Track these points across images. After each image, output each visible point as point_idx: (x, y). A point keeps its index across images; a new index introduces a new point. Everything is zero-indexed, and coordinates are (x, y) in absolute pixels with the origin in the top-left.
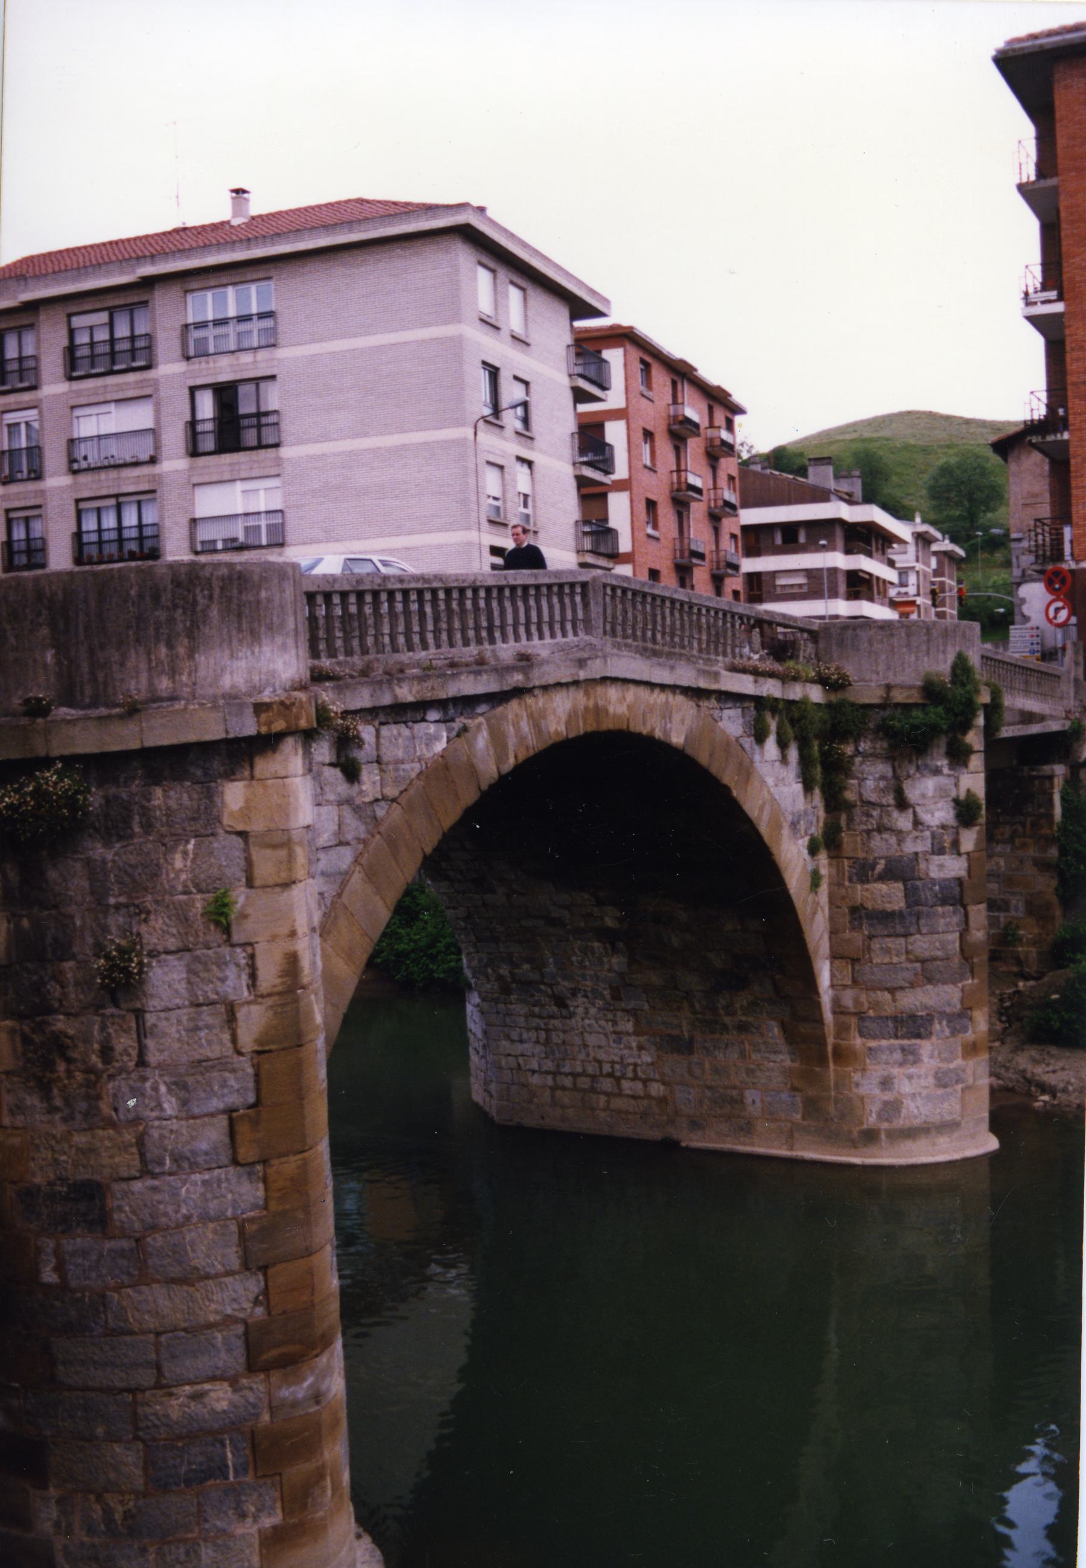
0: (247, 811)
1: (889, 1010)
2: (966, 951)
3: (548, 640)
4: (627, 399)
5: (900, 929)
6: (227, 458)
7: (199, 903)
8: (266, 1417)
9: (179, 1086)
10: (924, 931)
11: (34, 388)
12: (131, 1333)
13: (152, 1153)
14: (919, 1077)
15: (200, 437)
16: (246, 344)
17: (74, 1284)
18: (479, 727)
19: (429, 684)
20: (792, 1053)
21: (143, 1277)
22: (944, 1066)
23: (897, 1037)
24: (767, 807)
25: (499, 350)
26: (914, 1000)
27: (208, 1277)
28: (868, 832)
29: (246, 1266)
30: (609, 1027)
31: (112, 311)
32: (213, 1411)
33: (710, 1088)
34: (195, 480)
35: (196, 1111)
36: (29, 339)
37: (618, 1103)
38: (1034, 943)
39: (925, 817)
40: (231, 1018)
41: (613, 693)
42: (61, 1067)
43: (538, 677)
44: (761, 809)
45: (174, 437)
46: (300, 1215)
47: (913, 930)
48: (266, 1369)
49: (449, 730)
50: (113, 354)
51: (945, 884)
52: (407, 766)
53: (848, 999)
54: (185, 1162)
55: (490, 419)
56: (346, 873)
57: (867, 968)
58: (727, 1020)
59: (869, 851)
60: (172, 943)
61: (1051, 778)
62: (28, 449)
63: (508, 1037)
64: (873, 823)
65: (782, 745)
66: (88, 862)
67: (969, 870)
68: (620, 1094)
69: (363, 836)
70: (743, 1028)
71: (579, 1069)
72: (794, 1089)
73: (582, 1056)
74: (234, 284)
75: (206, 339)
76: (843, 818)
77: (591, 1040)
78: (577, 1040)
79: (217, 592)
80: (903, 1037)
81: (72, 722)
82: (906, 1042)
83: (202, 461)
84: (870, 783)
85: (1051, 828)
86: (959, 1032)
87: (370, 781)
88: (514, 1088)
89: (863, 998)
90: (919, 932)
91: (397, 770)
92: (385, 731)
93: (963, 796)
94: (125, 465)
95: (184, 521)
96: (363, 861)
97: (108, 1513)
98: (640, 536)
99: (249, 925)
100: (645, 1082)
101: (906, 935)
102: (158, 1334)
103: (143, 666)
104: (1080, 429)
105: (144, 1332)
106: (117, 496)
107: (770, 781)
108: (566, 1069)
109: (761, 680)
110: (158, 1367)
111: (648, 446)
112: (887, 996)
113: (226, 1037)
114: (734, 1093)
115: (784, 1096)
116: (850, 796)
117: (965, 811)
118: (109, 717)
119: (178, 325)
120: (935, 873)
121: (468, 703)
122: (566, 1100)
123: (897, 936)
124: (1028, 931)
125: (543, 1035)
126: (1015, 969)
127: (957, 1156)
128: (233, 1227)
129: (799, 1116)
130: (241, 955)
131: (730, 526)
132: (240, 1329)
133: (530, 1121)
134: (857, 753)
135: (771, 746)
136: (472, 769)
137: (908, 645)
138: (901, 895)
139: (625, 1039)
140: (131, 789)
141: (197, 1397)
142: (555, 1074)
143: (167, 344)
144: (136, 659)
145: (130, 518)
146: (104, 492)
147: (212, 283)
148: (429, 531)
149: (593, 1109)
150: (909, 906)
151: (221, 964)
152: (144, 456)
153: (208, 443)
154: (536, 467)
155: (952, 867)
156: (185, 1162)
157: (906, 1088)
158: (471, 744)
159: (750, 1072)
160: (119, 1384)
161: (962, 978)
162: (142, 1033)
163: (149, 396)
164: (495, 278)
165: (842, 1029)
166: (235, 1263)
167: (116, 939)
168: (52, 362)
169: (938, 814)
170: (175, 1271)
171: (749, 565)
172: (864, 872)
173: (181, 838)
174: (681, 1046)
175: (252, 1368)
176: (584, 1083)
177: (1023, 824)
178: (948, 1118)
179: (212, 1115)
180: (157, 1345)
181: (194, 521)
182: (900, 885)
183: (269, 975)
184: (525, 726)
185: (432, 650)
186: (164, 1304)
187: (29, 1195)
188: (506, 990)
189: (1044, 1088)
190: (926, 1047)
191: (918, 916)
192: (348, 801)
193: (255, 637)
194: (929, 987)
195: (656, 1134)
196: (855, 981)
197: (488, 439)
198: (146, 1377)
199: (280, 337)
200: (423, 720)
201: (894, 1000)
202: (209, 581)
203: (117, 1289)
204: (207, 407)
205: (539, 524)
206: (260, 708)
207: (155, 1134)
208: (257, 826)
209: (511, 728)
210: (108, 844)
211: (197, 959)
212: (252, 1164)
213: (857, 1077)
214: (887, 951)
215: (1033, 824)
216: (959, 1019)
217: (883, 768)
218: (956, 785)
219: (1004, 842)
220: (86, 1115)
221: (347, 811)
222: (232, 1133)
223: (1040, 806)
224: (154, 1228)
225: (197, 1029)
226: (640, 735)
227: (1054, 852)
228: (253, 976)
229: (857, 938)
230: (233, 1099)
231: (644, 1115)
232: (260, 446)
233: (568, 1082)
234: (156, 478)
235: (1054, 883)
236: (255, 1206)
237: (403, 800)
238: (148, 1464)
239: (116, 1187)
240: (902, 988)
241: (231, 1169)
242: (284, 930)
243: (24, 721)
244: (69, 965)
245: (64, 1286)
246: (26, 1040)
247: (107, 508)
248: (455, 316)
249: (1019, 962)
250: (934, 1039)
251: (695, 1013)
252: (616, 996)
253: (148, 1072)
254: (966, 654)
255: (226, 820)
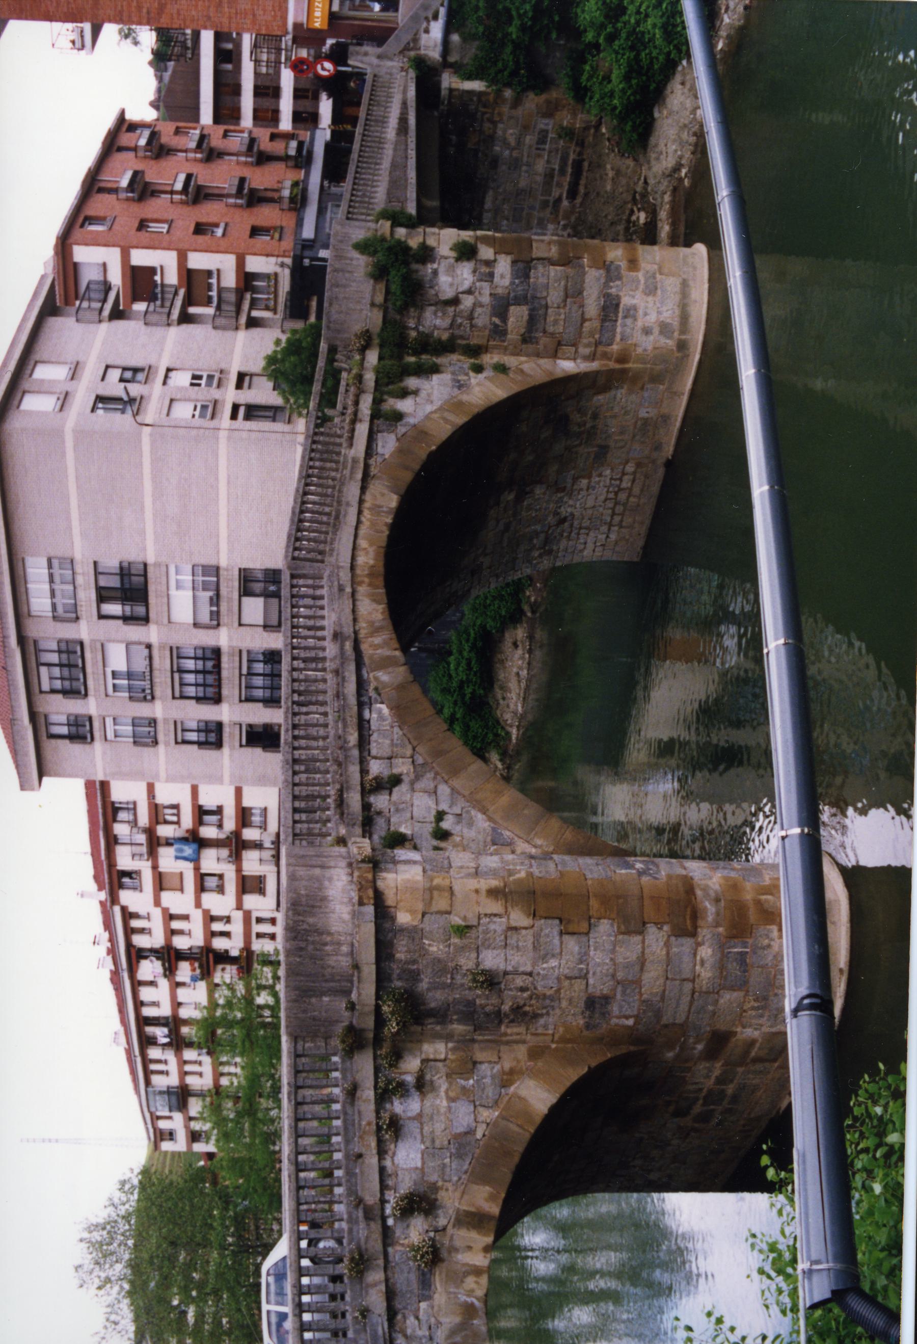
0: (412, 912)
1: (596, 324)
2: (564, 261)
3: (325, 612)
4: (114, 246)
5: (541, 312)
6: (152, 599)
7: (455, 940)
8: (721, 929)
9: (544, 958)
10: (545, 294)
11: (90, 719)
12: (664, 991)
13: (576, 973)
14: (646, 307)
15: (135, 614)
16: (70, 578)
17: (635, 1013)
18: (376, 679)
19: (349, 719)
20: (617, 388)
21: (638, 983)
22: (642, 287)
23: (616, 321)
24: (446, 414)
25: (83, 397)
26: (592, 307)
27: (643, 953)
28: (472, 326)
29: (641, 933)
30: (583, 493)
31: (39, 664)
32: (712, 956)
33: (634, 436)
34: (165, 621)
35: (558, 951)
36: (54, 718)
37: (636, 490)
38: (574, 115)
39: (466, 285)
40: (516, 929)
41: (361, 559)
42: (527, 1008)
43: (348, 630)
44: (446, 421)
45: (135, 632)
46: (621, 901)
47: (544, 303)
48: (695, 927)
49: (376, 702)
50: (70, 666)
51: (516, 274)
52: (396, 736)
53: (584, 351)
54: (583, 958)
55: (135, 408)
56: (453, 789)
57: (565, 336)
58: (588, 425)
59: (485, 327)
60: (474, 955)
61: (451, 90)
62: (134, 725)
63: (581, 551)
64: (466, 323)
65: (404, 394)
66: (429, 989)
67: (507, 253)
68: (631, 489)
69: (432, 775)
70: (595, 416)
71: (610, 511)
72: (642, 388)
73: (601, 509)
74: (26, 582)
75: (64, 604)
76: (459, 342)
77: (590, 503)
78: (590, 512)
79: (301, 918)
80: (617, 316)
81: (359, 994)
82: (620, 315)
83: (152, 615)
84: (438, 322)
85: (488, 94)
86: (619, 273)
87: (403, 767)
88: (617, 549)
89: (585, 341)
90: (545, 298)
91: (397, 745)
92: (374, 752)
93: (453, 254)
94: (151, 665)
95: (195, 631)
96: (446, 778)
97: (753, 1008)
98: (224, 244)
99: (470, 915)
100: (624, 474)
101: (547, 307)
102: (667, 978)
103: (335, 958)
104: (184, 20)
105: (665, 985)
106: (172, 672)
107: (429, 408)
108: (609, 519)
109: (360, 415)
110: (684, 980)
111: (151, 225)
112: (587, 324)
113: (524, 932)
114: (639, 423)
115: (646, 394)
116: (445, 336)
117: (466, 252)
118: (359, 977)
119: (52, 623)
120: (506, 282)
121: (361, 684)
122: (630, 520)
123: (546, 314)
124: (565, 119)
125: (582, 531)
126: (592, 131)
127: (706, 286)
128: (620, 937)
129: (661, 387)
130: (484, 920)
131: (216, 141)
132: (673, 939)
133: (641, 543)
134: (416, 329)
135: (405, 405)
136: (400, 688)
137: (345, 286)
138: (518, 308)
139: (593, 484)
140: (396, 969)
141: (703, 963)
142: (610, 525)
143: (67, 632)
144: (332, 961)
145: (190, 664)
146: (169, 680)
147: (24, 597)
148: (217, 465)
149: (638, 505)
150: (527, 304)
151: (486, 932)
152: (146, 652)
153: (140, 610)
154: (171, 366)
155: (504, 267)
156: (583, 958)
157: (652, 318)
158: (385, 685)
159: (626, 413)
160: (689, 998)
161: (582, 267)
162: (516, 972)
163: (102, 645)
164: (29, 392)
165: (606, 356)
166: (638, 938)
167: (467, 981)
168: (75, 706)
169: (465, 276)
170: (637, 968)
171: (247, 120)
172: (499, 332)
173: (422, 947)
174: (603, 452)
175: (693, 934)
176: (619, 509)
177: (484, 113)
178: (678, 289)
179: (561, 943)
180: (673, 980)
181: (196, 625)
182: (512, 308)
183: (495, 907)
184: (377, 640)
185: (328, 709)
186: (653, 974)
187: (588, 1026)
188: (550, 552)
189: (677, 168)
190: (626, 301)
191: (534, 297)
192: (412, 783)
193: (324, 899)
194: (585, 293)
195: (661, 472)
196: (573, 345)
197: (151, 413)
198: (688, 986)
199: (66, 555)
200: (369, 722)
201: (590, 320)
202: (295, 922)
203: (641, 994)
204: (114, 608)
205: (214, 368)
206: (361, 903)
207: (567, 971)
208: (420, 907)
209: (379, 651)
210: (421, 981)
211: (483, 944)
212: (590, 925)
213: (639, 350)
214: (556, 322)
215: (485, 106)
216: (611, 272)
217: (429, 313)
218: (446, 258)
219: (495, 127)
220: (552, 1000)
221: (419, 785)
222: (573, 934)
223: (472, 100)
224: (613, 976)
225: (517, 947)
226: (389, 537)
227: (508, 93)
228: (495, 915)
229: (544, 340)
230: (556, 932)
231: (647, 476)
232: (145, 575)
233: (617, 519)
234: (162, 647)
235: (531, 95)
236: (612, 925)
237: (415, 743)
238: (732, 989)
239: (590, 990)
240: (583, 313)
241: (591, 935)
242: (474, 895)
243: (356, 1013)
244: (478, 1002)
245: (636, 1017)
246: (512, 1021)
247: (181, 679)
248: (58, 433)
249: (586, 129)
250: (621, 294)
251: (580, 444)
252: (563, 489)
253: (535, 971)
254: (355, 241)
255: (415, 923)
